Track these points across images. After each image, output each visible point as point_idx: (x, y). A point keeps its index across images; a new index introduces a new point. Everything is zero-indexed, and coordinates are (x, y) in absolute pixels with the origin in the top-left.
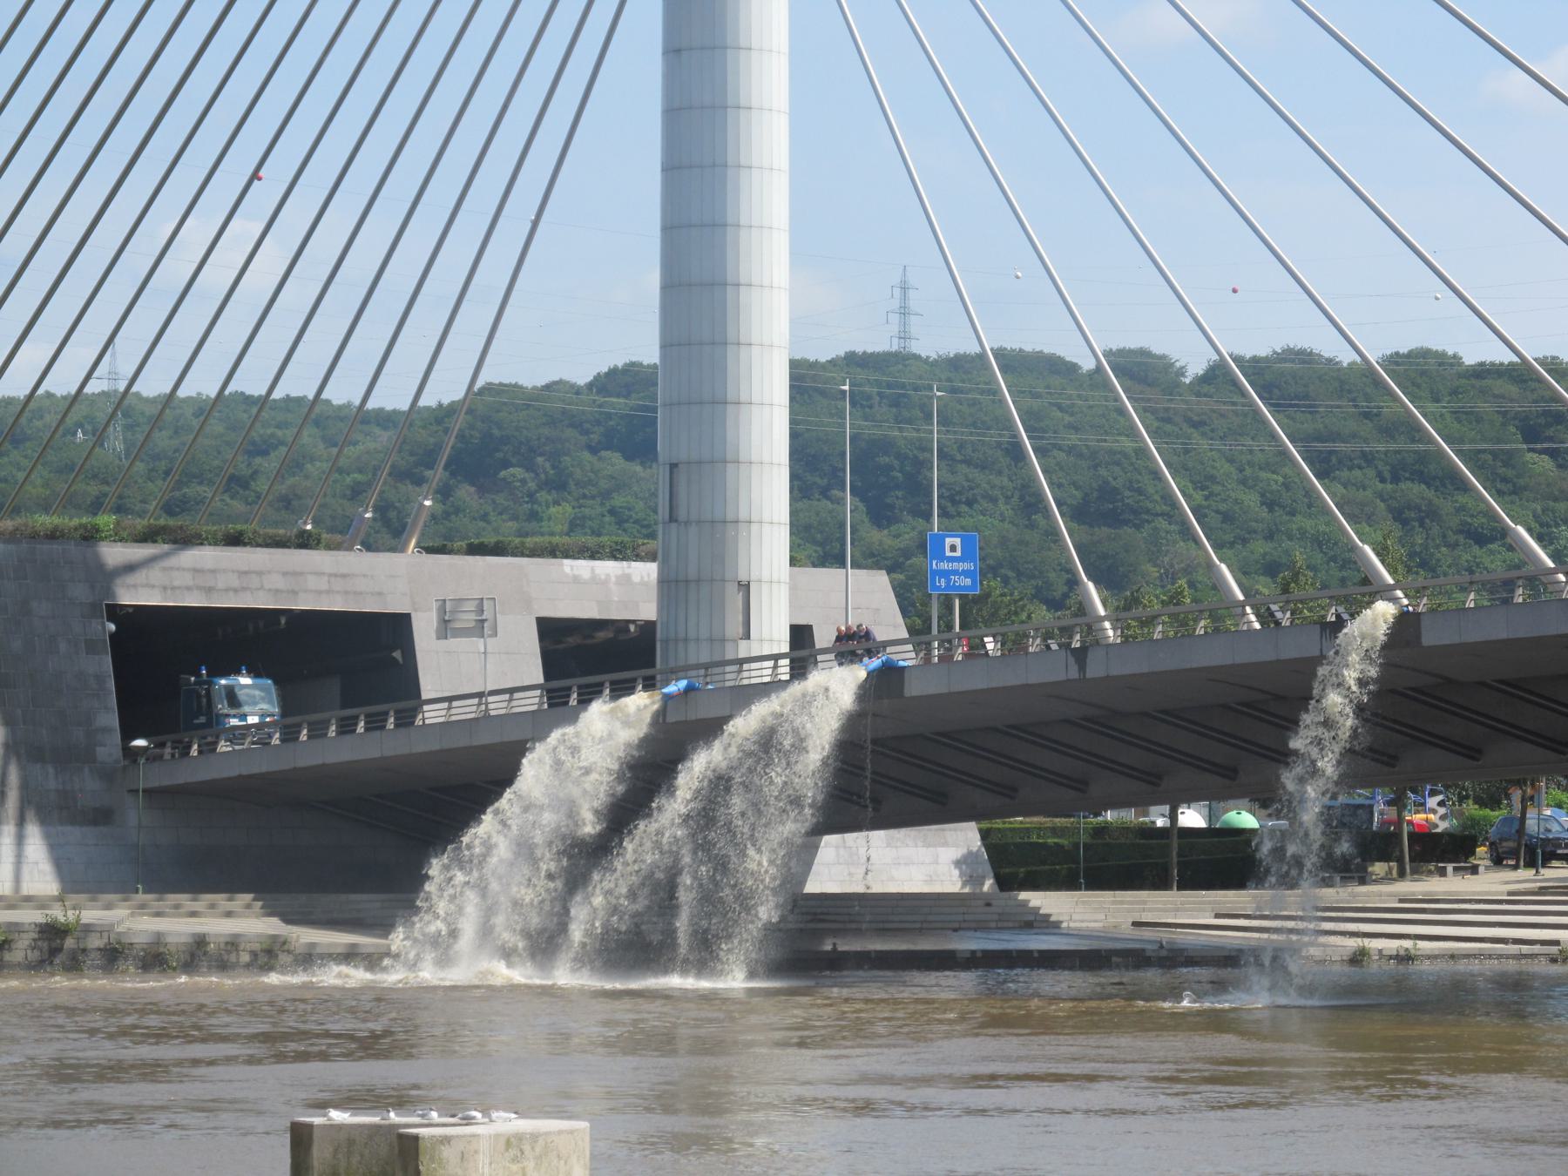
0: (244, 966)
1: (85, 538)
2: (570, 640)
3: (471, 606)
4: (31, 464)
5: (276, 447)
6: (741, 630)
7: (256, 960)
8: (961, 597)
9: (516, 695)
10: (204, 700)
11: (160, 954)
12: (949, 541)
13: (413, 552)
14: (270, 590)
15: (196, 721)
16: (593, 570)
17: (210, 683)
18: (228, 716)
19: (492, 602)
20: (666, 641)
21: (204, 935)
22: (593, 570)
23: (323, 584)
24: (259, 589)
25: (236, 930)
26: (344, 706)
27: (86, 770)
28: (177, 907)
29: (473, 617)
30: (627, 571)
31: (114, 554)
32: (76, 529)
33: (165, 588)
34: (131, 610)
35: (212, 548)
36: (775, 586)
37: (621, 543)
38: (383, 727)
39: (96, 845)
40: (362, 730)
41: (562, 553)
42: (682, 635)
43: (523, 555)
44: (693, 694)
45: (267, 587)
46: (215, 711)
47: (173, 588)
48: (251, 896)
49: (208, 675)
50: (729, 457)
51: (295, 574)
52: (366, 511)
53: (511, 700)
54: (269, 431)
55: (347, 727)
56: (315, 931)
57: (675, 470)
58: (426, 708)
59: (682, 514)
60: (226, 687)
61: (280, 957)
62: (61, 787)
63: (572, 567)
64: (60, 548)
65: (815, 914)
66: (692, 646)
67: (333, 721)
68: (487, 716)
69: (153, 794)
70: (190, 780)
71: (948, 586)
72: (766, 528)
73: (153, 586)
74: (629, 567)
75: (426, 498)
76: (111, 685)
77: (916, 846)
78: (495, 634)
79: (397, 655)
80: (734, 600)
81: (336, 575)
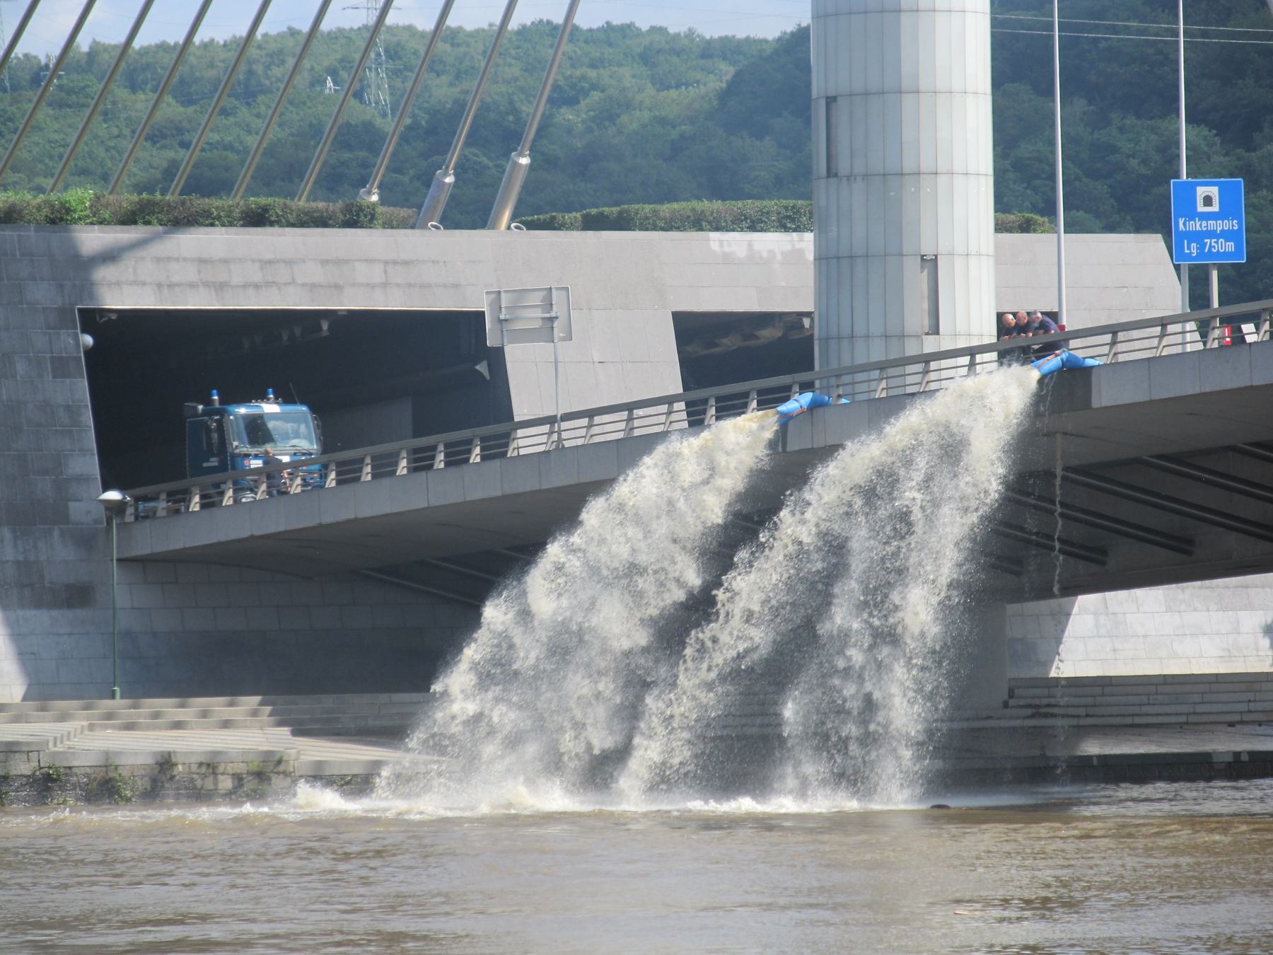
0: (226, 795)
1: (53, 222)
2: (725, 341)
3: (536, 299)
4: (265, 125)
5: (586, 94)
6: (926, 322)
7: (241, 786)
8: (1220, 268)
9: (597, 419)
10: (215, 436)
11: (111, 779)
12: (1201, 191)
13: (509, 228)
14: (304, 285)
15: (205, 465)
16: (750, 245)
17: (222, 413)
18: (247, 456)
19: (564, 293)
20: (826, 340)
21: (169, 754)
22: (750, 245)
23: (376, 273)
24: (290, 283)
25: (218, 746)
26: (417, 433)
27: (56, 533)
28: (156, 715)
29: (539, 313)
30: (798, 246)
31: (91, 239)
32: (39, 208)
33: (160, 286)
34: (114, 317)
35: (224, 229)
36: (973, 262)
37: (793, 207)
38: (430, 467)
39: (70, 634)
40: (405, 471)
41: (709, 222)
42: (846, 331)
43: (655, 228)
44: (820, 411)
45: (300, 280)
46: (230, 450)
47: (171, 286)
48: (257, 699)
49: (222, 402)
50: (906, 84)
51: (338, 262)
52: (446, 174)
53: (590, 426)
54: (578, 73)
55: (421, 462)
56: (333, 745)
57: (834, 105)
58: (520, 433)
59: (843, 166)
60: (245, 417)
61: (274, 780)
62: (21, 558)
63: (721, 242)
64: (15, 234)
65: (1038, 706)
66: (860, 346)
67: (404, 454)
68: (560, 448)
69: (135, 563)
70: (190, 544)
71: (1201, 254)
72: (959, 181)
73: (144, 284)
74: (801, 240)
75: (521, 155)
76: (88, 418)
77: (1208, 610)
78: (569, 337)
79: (482, 367)
80: (917, 281)
81: (395, 263)
